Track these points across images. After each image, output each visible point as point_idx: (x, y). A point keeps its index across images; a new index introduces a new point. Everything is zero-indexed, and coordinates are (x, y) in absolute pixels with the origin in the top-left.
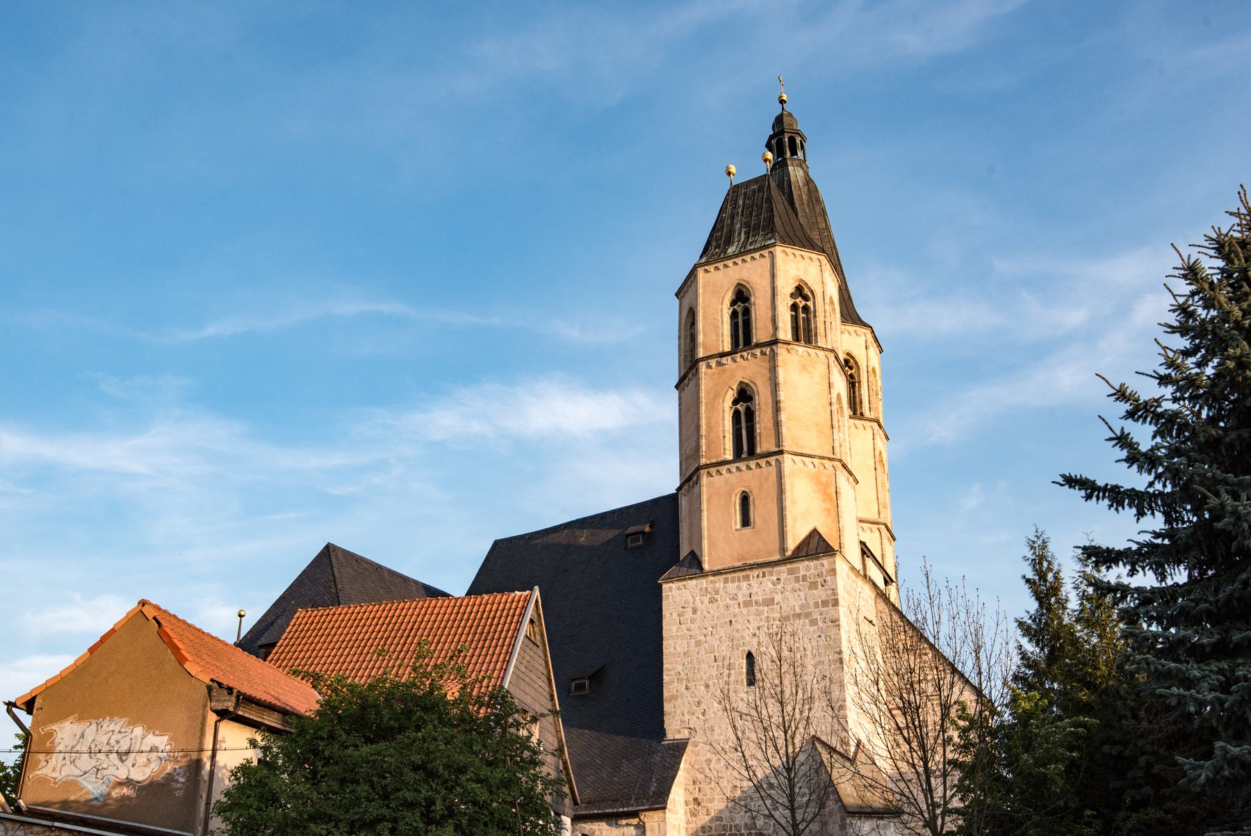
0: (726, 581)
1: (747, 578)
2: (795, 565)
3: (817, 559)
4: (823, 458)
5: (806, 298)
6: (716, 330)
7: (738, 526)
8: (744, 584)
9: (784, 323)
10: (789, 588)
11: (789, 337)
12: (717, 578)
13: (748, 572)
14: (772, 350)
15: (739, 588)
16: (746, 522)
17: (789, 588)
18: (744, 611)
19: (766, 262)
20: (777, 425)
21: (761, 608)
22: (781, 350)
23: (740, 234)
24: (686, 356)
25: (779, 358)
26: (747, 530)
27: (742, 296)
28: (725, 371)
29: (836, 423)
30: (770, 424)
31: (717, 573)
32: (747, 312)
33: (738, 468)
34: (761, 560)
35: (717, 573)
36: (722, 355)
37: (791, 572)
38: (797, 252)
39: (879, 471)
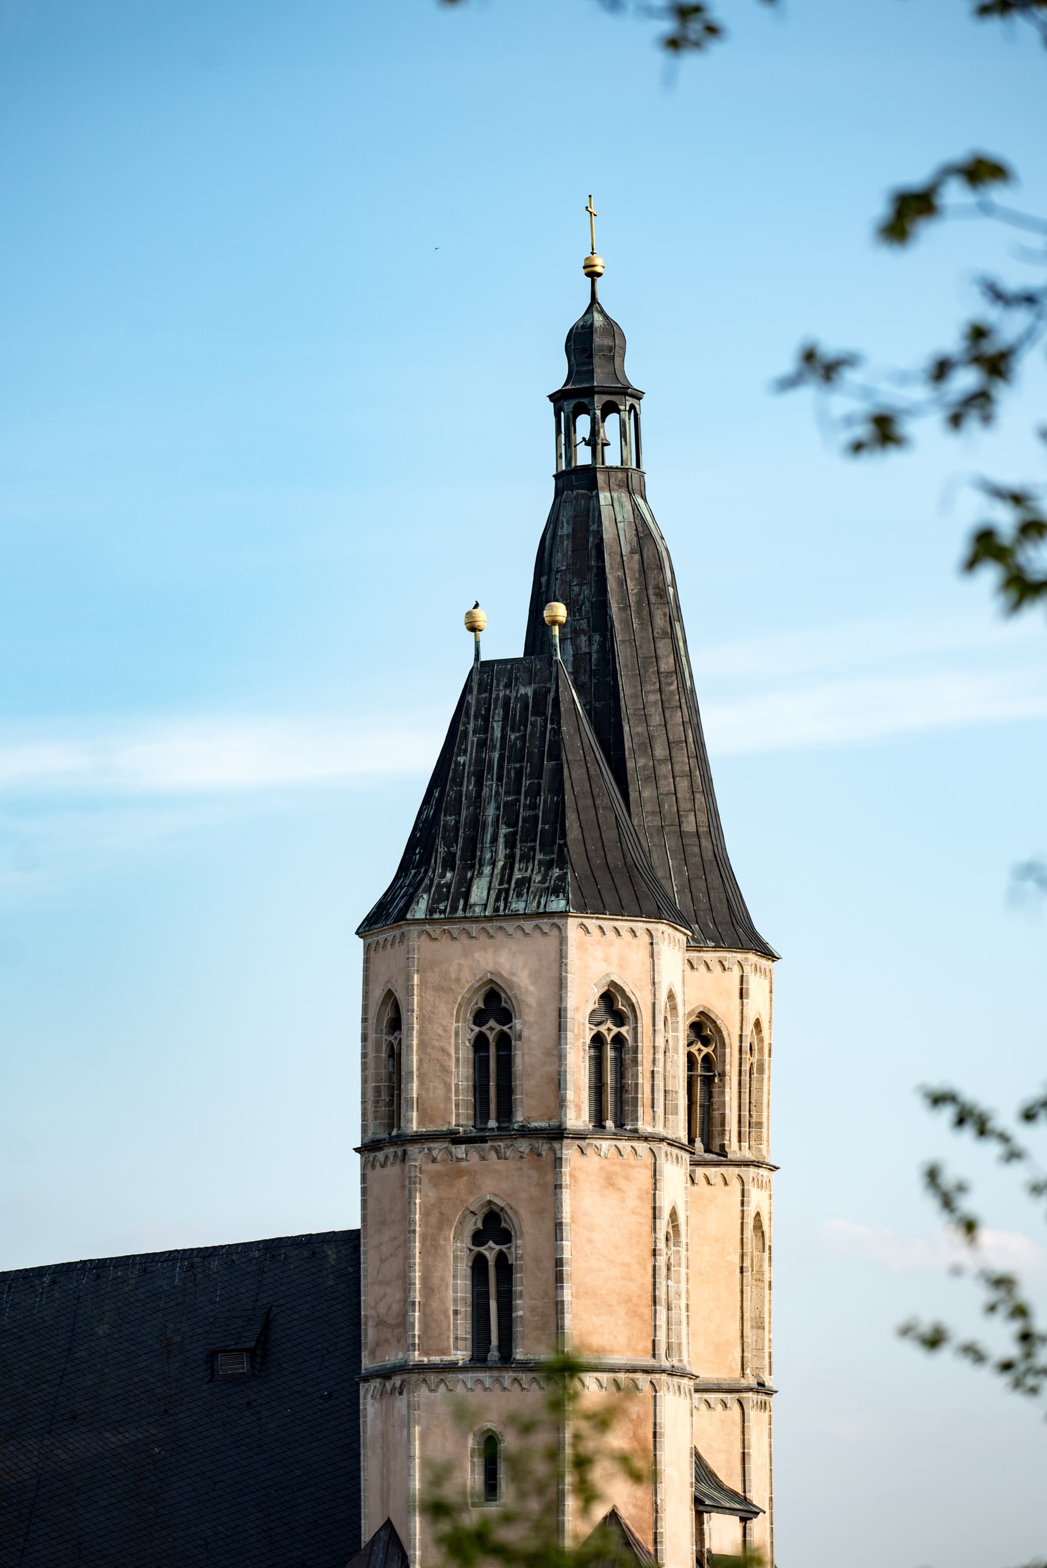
4: (634, 1370)
5: (619, 1019)
6: (441, 1085)
9: (578, 1088)
19: (553, 941)
22: (569, 1151)
23: (494, 840)
24: (377, 1090)
25: (566, 1170)
27: (494, 1005)
29: (661, 1294)
32: (505, 1042)
36: (454, 1138)
38: (605, 924)
39: (747, 1274)
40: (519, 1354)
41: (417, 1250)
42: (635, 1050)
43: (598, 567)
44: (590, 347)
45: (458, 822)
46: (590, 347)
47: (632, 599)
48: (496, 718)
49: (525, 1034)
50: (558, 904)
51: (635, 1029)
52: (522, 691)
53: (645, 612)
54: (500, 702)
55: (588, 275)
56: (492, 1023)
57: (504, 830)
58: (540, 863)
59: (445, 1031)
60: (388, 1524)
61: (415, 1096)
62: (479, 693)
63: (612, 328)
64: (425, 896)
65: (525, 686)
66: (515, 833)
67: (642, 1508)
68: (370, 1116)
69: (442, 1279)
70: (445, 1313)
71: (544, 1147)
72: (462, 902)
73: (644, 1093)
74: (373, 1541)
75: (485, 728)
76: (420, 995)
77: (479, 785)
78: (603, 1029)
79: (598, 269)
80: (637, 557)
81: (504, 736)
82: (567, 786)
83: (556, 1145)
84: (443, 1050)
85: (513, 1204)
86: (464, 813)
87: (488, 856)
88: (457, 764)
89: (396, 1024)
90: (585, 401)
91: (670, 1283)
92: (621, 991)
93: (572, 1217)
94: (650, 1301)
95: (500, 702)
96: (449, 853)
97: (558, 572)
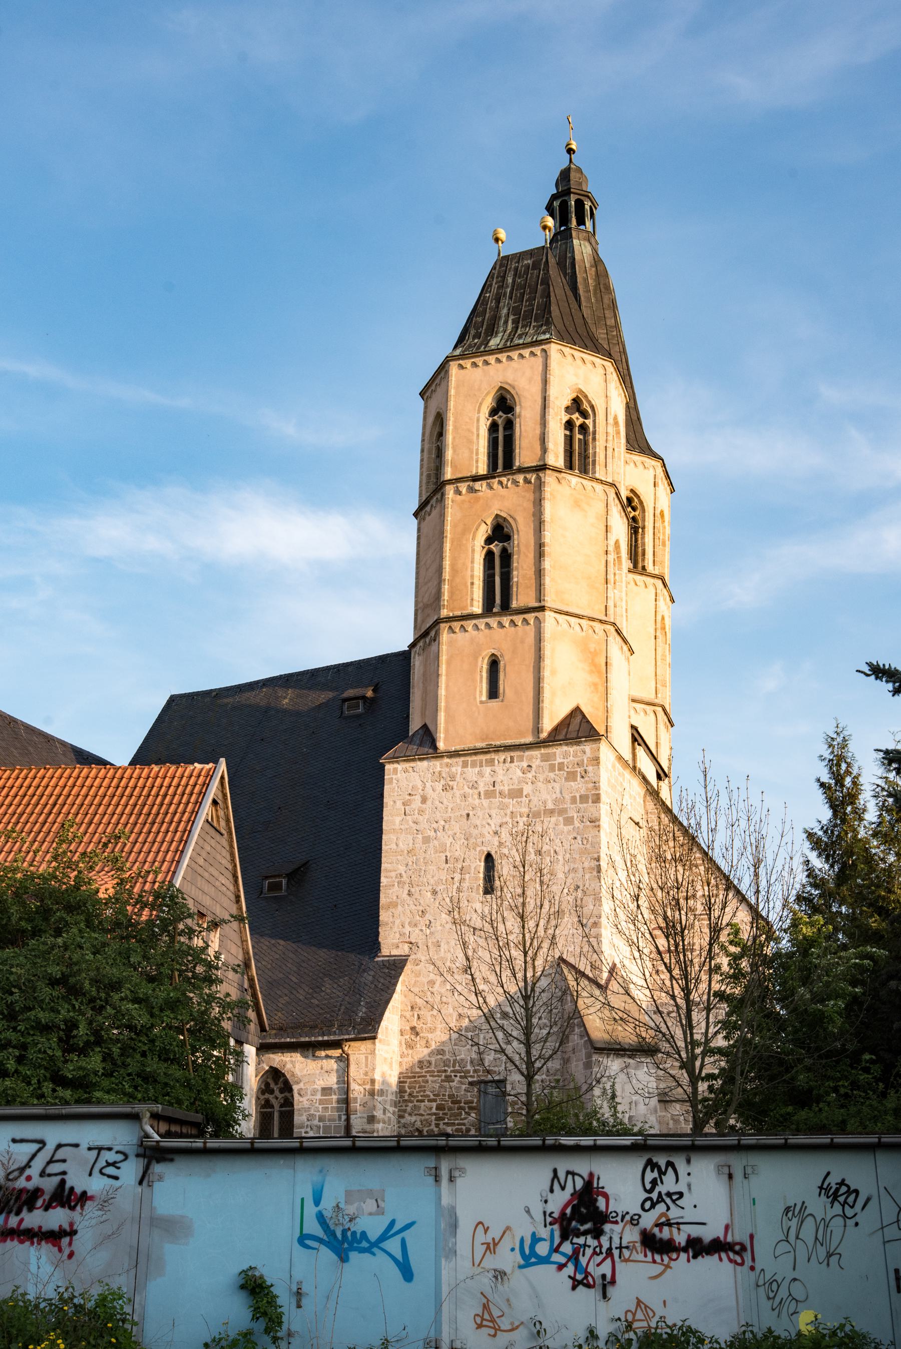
5: (584, 415)
9: (556, 444)
19: (539, 361)
22: (549, 478)
23: (506, 322)
24: (429, 476)
29: (611, 577)
36: (476, 478)
38: (576, 354)
40: (514, 604)
41: (448, 549)
42: (594, 433)
47: (591, 288)
49: (523, 414)
51: (594, 421)
52: (526, 262)
53: (599, 295)
58: (534, 327)
59: (470, 419)
60: (425, 727)
61: (450, 459)
63: (579, 170)
67: (597, 709)
68: (424, 488)
69: (464, 564)
70: (465, 585)
71: (533, 477)
73: (600, 458)
74: (413, 735)
76: (455, 401)
80: (594, 269)
81: (514, 281)
82: (552, 294)
83: (541, 475)
84: (469, 430)
86: (487, 315)
89: (441, 434)
91: (616, 591)
92: (586, 397)
93: (551, 519)
94: (603, 581)
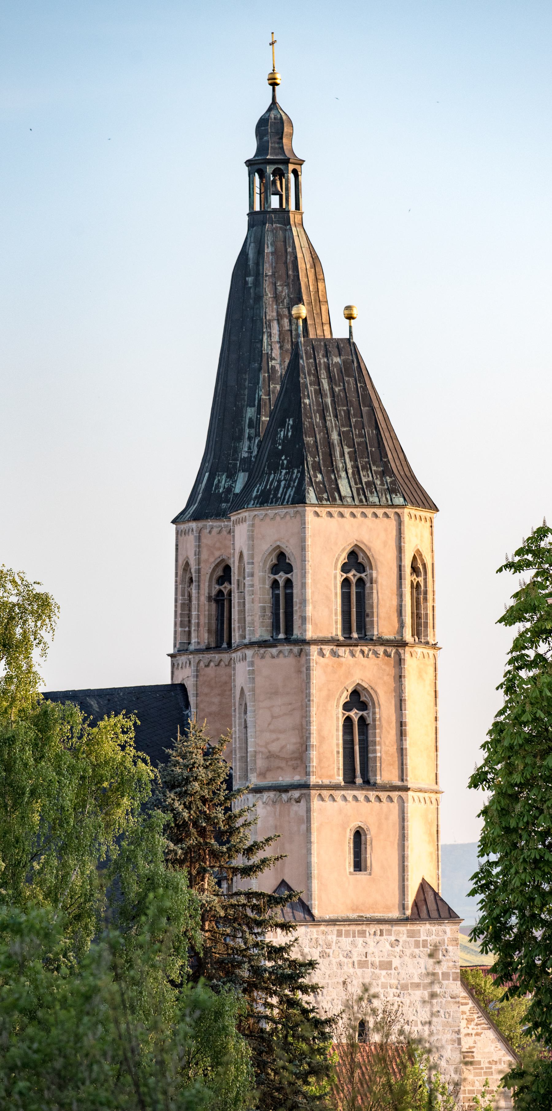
0: (339, 934)
1: (363, 934)
2: (415, 927)
3: (440, 924)
7: (352, 869)
8: (360, 941)
10: (408, 952)
11: (336, 630)
12: (330, 928)
13: (364, 927)
14: (398, 654)
15: (353, 943)
16: (359, 865)
17: (408, 952)
18: (359, 971)
20: (402, 752)
21: (377, 971)
23: (343, 455)
26: (361, 876)
27: (282, 562)
28: (340, 665)
30: (393, 749)
31: (333, 922)
33: (355, 798)
34: (378, 915)
35: (333, 922)
37: (411, 934)
42: (426, 593)
43: (294, 276)
44: (272, 128)
45: (316, 441)
46: (272, 128)
48: (323, 376)
50: (399, 500)
54: (322, 366)
55: (270, 84)
56: (353, 572)
57: (347, 450)
62: (307, 359)
64: (311, 488)
65: (336, 357)
66: (355, 452)
70: (332, 752)
71: (392, 651)
72: (336, 495)
75: (318, 382)
77: (324, 418)
78: (350, 575)
79: (278, 81)
81: (332, 390)
83: (401, 651)
84: (327, 587)
85: (373, 686)
86: (318, 436)
87: (341, 465)
88: (305, 404)
90: (281, 167)
95: (322, 366)
96: (314, 461)
97: (266, 276)
